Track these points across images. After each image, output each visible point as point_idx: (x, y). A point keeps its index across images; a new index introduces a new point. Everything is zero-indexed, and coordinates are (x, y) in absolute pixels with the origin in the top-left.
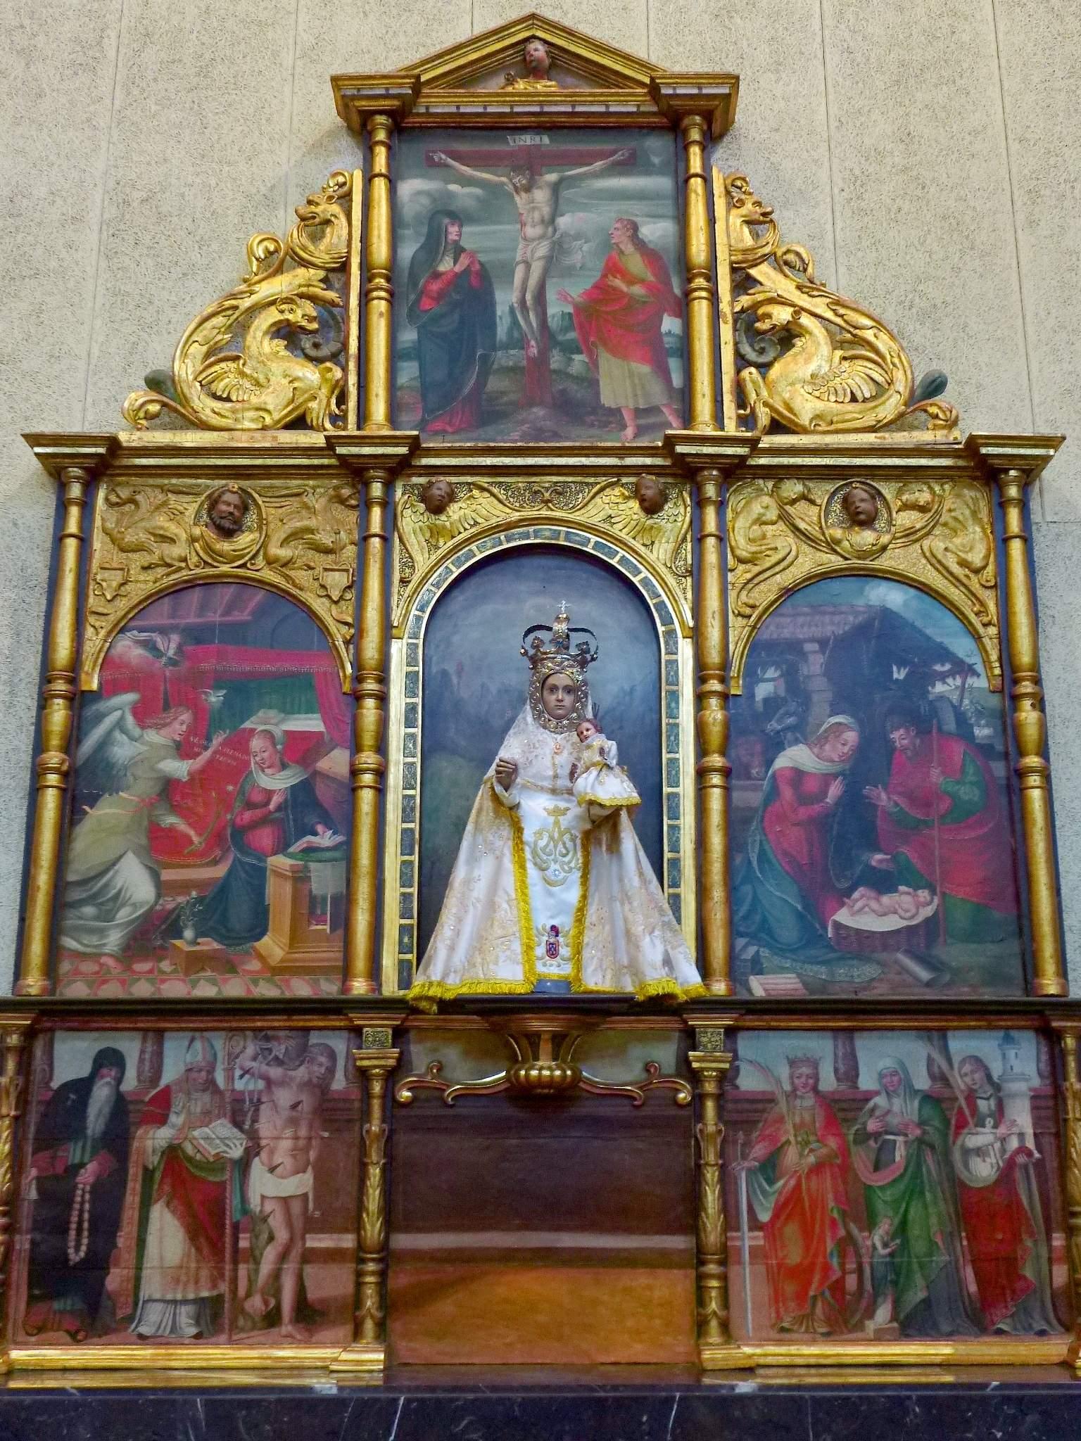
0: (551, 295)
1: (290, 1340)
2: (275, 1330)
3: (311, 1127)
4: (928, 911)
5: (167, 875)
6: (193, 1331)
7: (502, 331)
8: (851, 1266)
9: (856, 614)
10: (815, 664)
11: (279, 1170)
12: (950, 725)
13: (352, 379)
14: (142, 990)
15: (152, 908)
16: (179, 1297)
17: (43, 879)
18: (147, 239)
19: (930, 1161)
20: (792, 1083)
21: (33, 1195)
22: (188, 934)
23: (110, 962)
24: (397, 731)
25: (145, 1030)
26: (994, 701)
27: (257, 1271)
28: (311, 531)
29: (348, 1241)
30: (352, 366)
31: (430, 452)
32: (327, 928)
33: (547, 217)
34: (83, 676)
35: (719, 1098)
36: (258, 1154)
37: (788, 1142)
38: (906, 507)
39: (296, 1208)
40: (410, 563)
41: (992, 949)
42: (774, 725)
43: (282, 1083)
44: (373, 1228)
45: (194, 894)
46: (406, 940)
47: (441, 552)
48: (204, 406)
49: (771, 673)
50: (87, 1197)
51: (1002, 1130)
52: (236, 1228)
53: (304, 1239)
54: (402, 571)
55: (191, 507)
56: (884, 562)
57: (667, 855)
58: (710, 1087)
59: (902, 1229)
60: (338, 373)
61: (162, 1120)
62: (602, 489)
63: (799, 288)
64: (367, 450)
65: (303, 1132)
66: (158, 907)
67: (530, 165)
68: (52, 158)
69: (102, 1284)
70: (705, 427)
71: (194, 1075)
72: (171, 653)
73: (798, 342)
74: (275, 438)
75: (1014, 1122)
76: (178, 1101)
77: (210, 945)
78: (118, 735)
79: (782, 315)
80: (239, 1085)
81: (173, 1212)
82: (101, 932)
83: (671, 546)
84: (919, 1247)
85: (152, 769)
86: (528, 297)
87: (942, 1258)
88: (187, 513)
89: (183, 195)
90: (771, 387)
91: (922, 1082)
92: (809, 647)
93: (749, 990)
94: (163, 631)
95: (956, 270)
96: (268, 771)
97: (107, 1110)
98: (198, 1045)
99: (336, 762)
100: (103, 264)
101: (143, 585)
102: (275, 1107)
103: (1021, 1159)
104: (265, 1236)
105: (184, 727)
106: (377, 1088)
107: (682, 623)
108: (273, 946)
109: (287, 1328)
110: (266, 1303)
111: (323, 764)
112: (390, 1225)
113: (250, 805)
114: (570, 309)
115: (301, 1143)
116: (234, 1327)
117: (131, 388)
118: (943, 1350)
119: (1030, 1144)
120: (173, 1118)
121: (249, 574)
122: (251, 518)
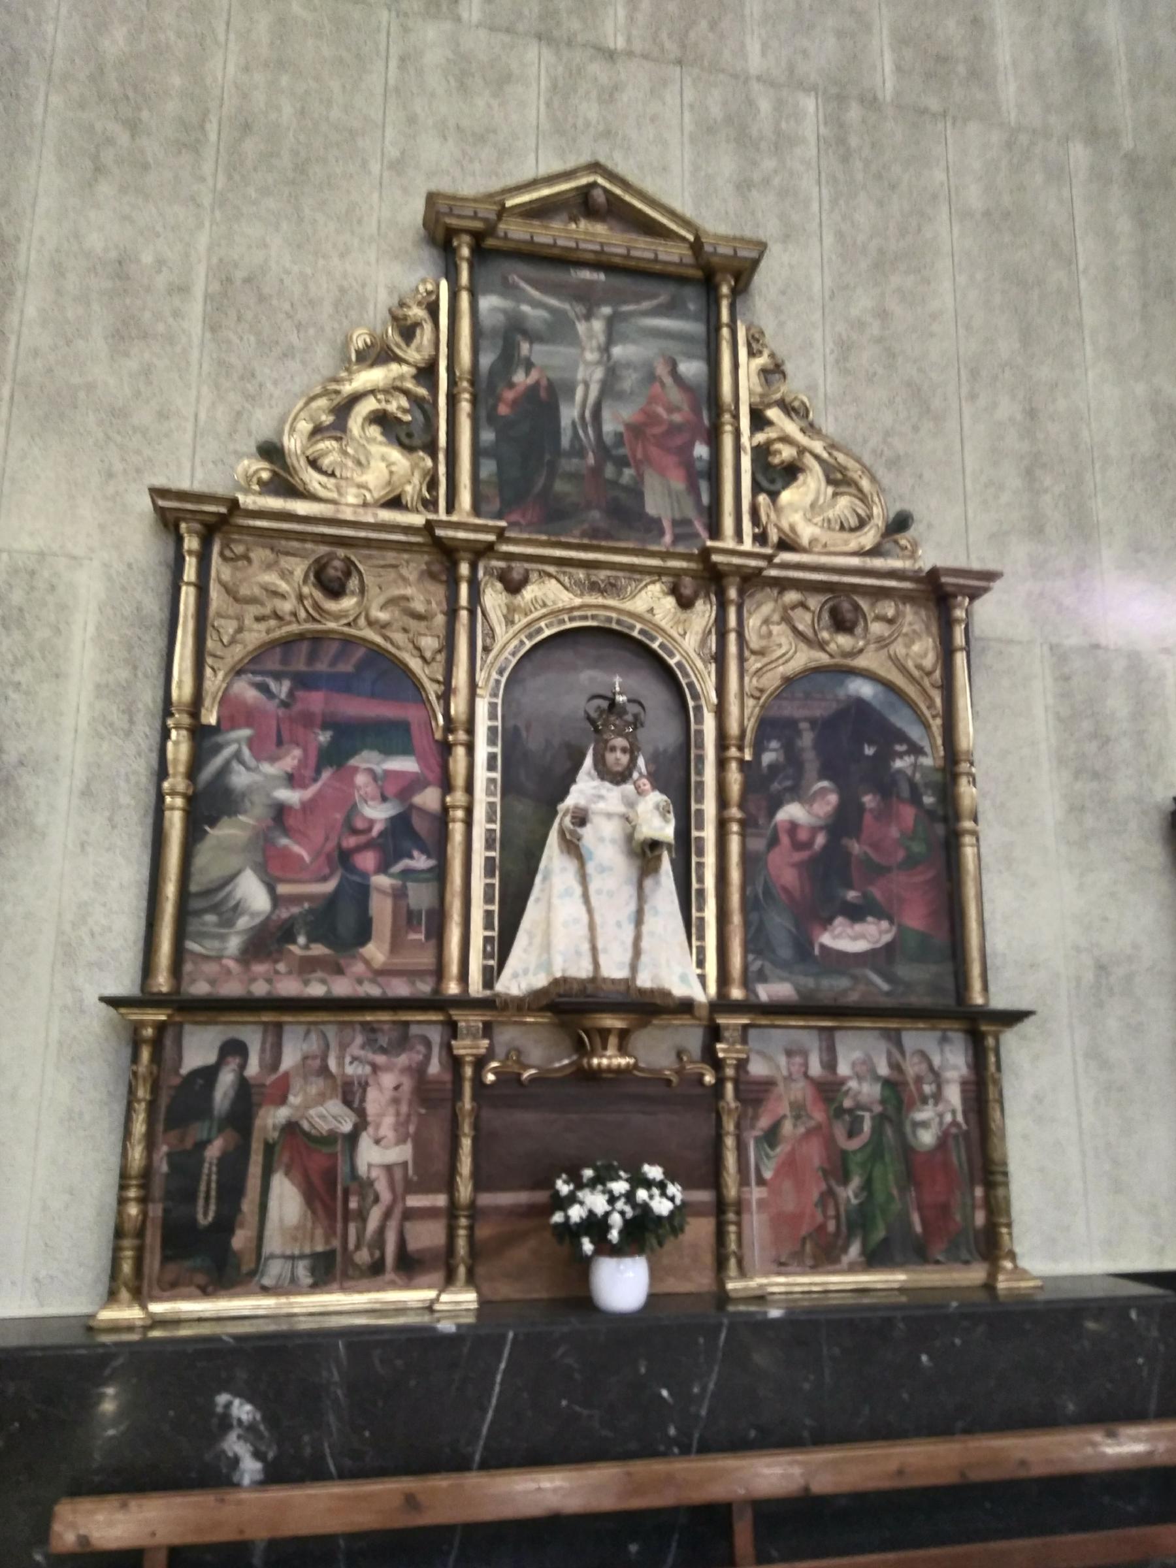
0: (606, 414)
1: (393, 1285)
2: (380, 1278)
3: (410, 1104)
4: (887, 938)
5: (282, 889)
6: (309, 1281)
7: (565, 441)
8: (831, 1212)
9: (838, 701)
10: (807, 739)
11: (383, 1143)
12: (905, 792)
13: (442, 469)
14: (260, 989)
15: (268, 918)
16: (297, 1252)
17: (170, 889)
18: (249, 315)
19: (889, 1131)
20: (789, 1069)
21: (165, 1168)
22: (302, 940)
23: (231, 964)
24: (481, 774)
25: (265, 1024)
26: (938, 777)
27: (364, 1228)
28: (407, 599)
29: (441, 1200)
30: (442, 457)
31: (509, 541)
32: (422, 937)
33: (603, 345)
34: (203, 711)
35: (736, 1082)
36: (365, 1129)
37: (784, 1117)
38: (878, 618)
39: (398, 1174)
40: (491, 634)
41: (934, 968)
42: (776, 786)
43: (388, 1068)
44: (465, 1191)
45: (306, 905)
46: (489, 948)
47: (517, 627)
48: (312, 480)
49: (774, 744)
50: (214, 1169)
51: (940, 1108)
52: (346, 1194)
53: (404, 1199)
54: (484, 640)
55: (299, 568)
56: (861, 662)
57: (695, 885)
58: (730, 1072)
59: (867, 1185)
60: (429, 463)
61: (283, 1100)
62: (646, 586)
63: (803, 430)
64: (461, 535)
65: (404, 1109)
66: (274, 917)
67: (587, 299)
68: (159, 228)
69: (228, 1243)
70: (729, 543)
71: (309, 1062)
72: (283, 696)
73: (801, 477)
74: (375, 515)
75: (948, 1102)
76: (296, 1083)
77: (319, 950)
78: (236, 766)
79: (786, 453)
80: (350, 1070)
81: (291, 1180)
82: (223, 938)
83: (699, 637)
84: (880, 1197)
85: (268, 795)
86: (588, 414)
87: (896, 1206)
88: (296, 573)
89: (282, 281)
90: (778, 510)
91: (883, 1070)
92: (804, 725)
93: (757, 996)
94: (278, 676)
95: (916, 429)
96: (370, 803)
97: (231, 1093)
98: (313, 1036)
99: (429, 798)
100: (208, 335)
101: (256, 635)
102: (380, 1088)
103: (954, 1130)
104: (371, 1198)
105: (296, 762)
106: (468, 1071)
107: (707, 701)
108: (376, 952)
109: (389, 1275)
110: (372, 1255)
111: (418, 800)
112: (480, 1182)
113: (355, 832)
114: (621, 428)
115: (402, 1118)
116: (345, 1276)
117: (240, 456)
118: (897, 1278)
119: (960, 1118)
120: (292, 1099)
121: (353, 631)
122: (353, 583)
